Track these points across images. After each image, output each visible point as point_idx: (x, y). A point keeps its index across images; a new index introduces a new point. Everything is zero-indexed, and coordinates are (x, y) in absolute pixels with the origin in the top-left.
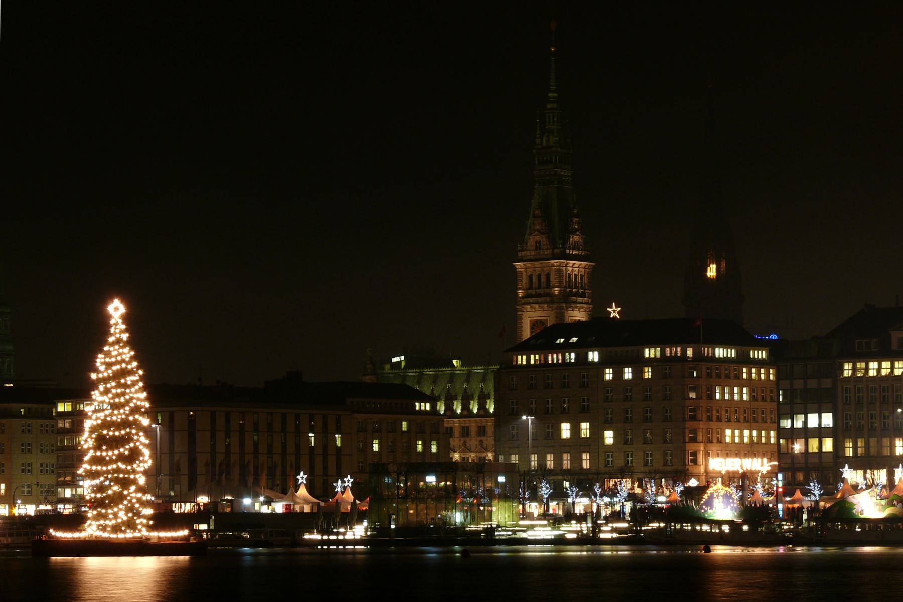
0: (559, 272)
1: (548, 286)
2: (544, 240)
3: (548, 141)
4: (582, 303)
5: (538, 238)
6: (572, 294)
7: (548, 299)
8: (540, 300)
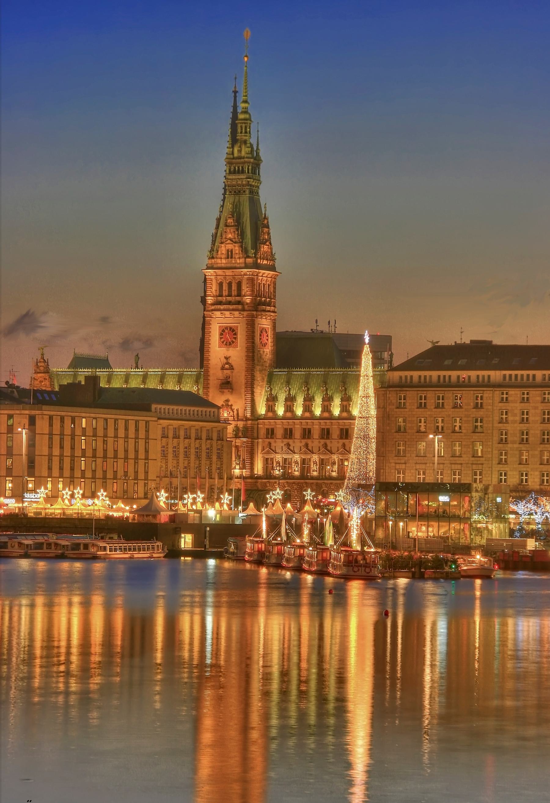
0: (252, 281)
1: (239, 295)
2: (237, 249)
3: (240, 151)
4: (269, 311)
5: (230, 247)
6: (261, 303)
7: (240, 307)
8: (231, 307)
